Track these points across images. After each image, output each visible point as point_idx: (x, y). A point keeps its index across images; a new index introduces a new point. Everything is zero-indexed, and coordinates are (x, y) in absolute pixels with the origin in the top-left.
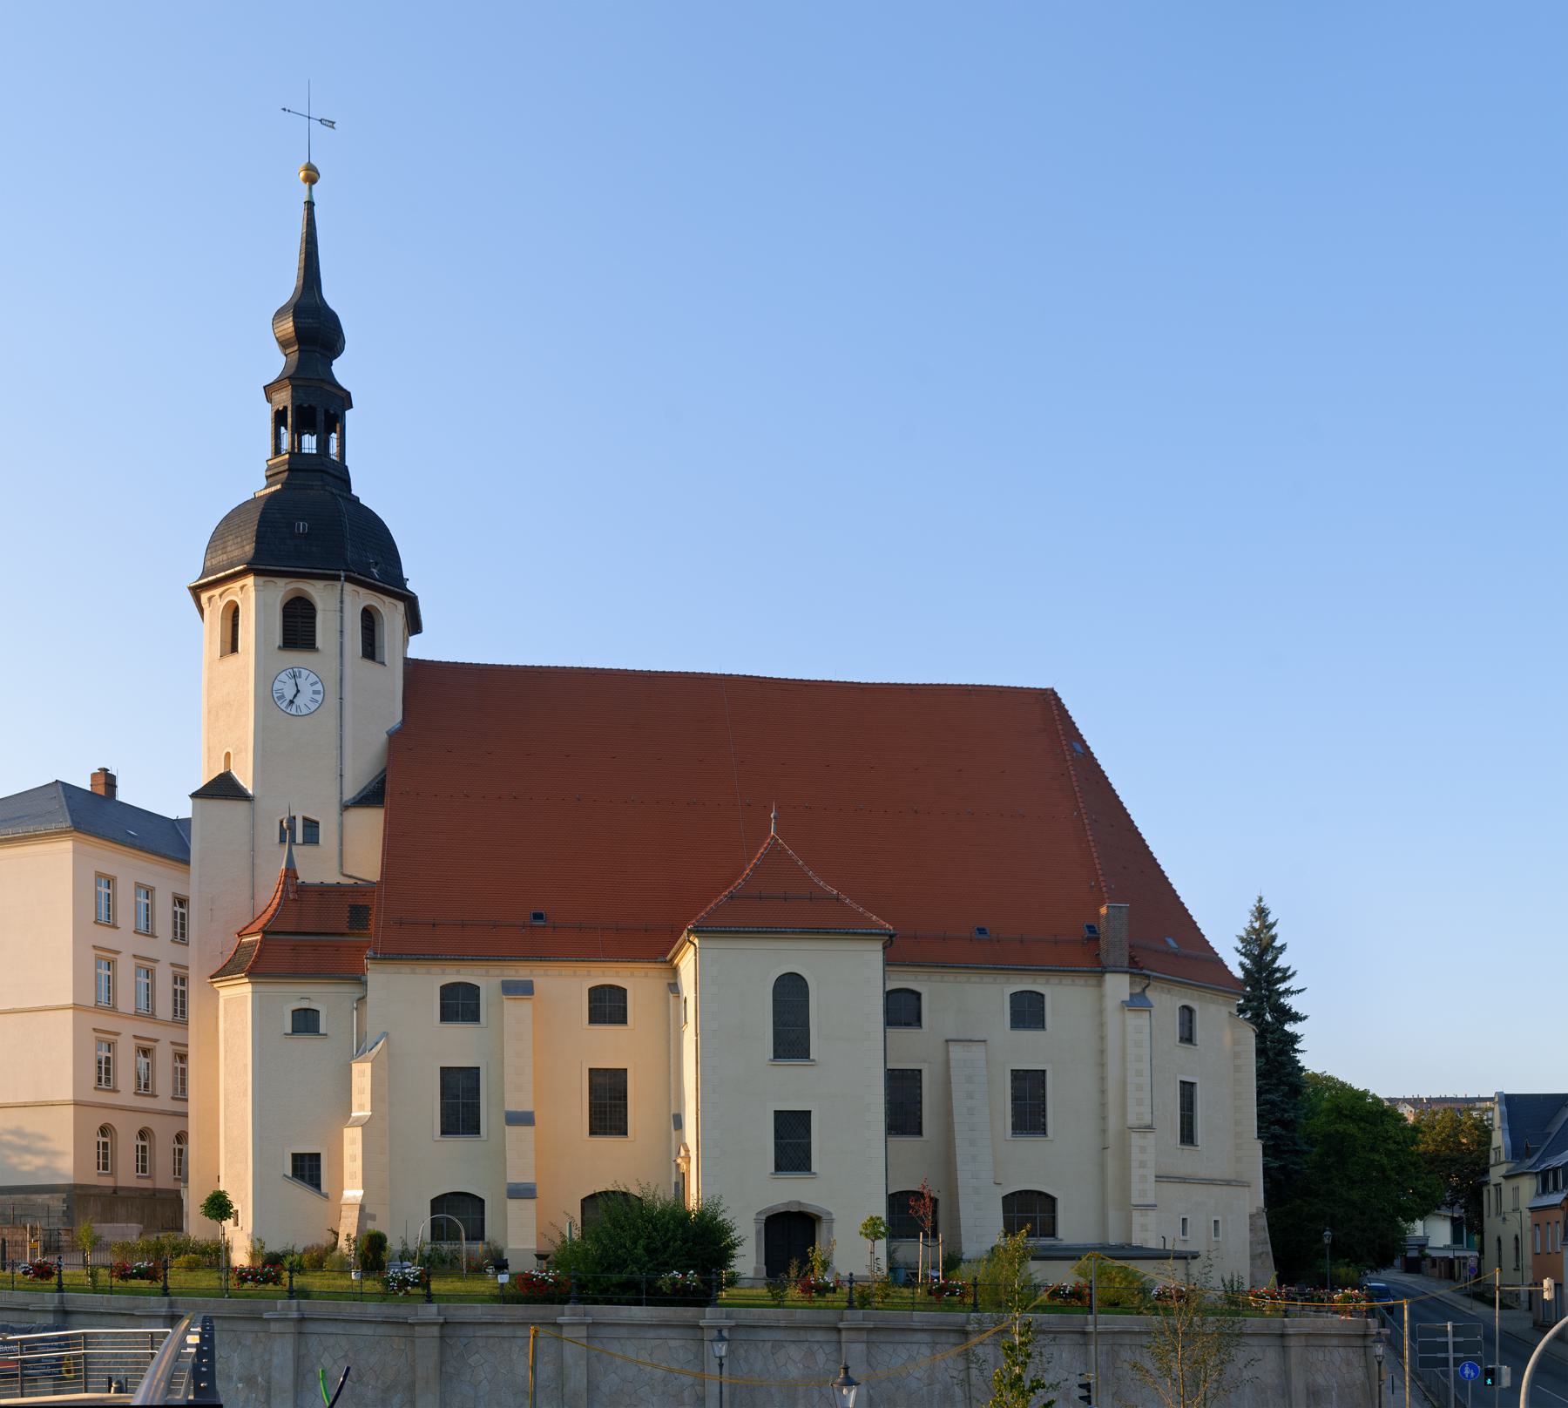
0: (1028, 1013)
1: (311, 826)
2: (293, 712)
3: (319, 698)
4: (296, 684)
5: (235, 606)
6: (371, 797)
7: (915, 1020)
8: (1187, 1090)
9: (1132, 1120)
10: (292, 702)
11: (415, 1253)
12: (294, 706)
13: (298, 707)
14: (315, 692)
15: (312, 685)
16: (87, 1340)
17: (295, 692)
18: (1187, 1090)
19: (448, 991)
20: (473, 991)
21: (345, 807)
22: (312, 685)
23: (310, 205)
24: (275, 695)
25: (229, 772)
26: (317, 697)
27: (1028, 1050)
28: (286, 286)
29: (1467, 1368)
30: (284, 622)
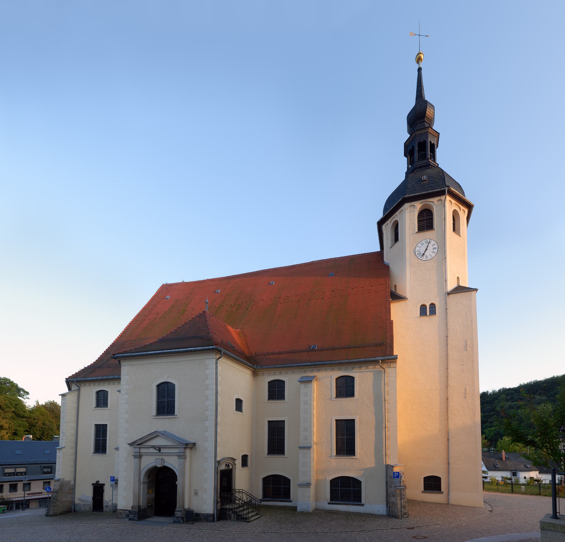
1: (433, 306)
2: (424, 259)
3: (436, 251)
4: (428, 246)
5: (397, 223)
10: (424, 254)
11: (214, 514)
12: (425, 256)
13: (426, 256)
14: (434, 249)
15: (433, 246)
19: (272, 384)
22: (433, 246)
23: (420, 70)
24: (416, 253)
25: (459, 285)
26: (434, 250)
29: (47, 488)
30: (432, 221)
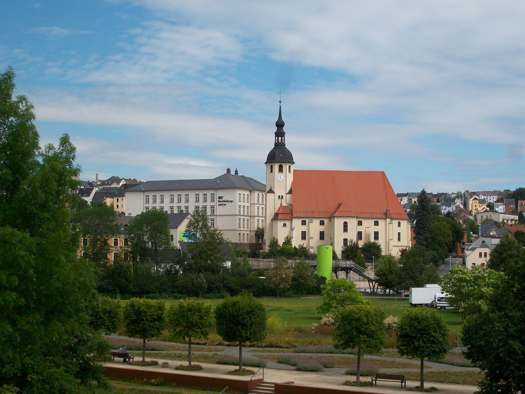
0: (376, 224)
1: (282, 196)
6: (290, 192)
7: (361, 225)
8: (399, 234)
9: (390, 239)
16: (347, 383)
17: (13, 391)
18: (399, 234)
20: (285, 224)
21: (287, 194)
23: (280, 106)
27: (376, 228)
28: (277, 119)
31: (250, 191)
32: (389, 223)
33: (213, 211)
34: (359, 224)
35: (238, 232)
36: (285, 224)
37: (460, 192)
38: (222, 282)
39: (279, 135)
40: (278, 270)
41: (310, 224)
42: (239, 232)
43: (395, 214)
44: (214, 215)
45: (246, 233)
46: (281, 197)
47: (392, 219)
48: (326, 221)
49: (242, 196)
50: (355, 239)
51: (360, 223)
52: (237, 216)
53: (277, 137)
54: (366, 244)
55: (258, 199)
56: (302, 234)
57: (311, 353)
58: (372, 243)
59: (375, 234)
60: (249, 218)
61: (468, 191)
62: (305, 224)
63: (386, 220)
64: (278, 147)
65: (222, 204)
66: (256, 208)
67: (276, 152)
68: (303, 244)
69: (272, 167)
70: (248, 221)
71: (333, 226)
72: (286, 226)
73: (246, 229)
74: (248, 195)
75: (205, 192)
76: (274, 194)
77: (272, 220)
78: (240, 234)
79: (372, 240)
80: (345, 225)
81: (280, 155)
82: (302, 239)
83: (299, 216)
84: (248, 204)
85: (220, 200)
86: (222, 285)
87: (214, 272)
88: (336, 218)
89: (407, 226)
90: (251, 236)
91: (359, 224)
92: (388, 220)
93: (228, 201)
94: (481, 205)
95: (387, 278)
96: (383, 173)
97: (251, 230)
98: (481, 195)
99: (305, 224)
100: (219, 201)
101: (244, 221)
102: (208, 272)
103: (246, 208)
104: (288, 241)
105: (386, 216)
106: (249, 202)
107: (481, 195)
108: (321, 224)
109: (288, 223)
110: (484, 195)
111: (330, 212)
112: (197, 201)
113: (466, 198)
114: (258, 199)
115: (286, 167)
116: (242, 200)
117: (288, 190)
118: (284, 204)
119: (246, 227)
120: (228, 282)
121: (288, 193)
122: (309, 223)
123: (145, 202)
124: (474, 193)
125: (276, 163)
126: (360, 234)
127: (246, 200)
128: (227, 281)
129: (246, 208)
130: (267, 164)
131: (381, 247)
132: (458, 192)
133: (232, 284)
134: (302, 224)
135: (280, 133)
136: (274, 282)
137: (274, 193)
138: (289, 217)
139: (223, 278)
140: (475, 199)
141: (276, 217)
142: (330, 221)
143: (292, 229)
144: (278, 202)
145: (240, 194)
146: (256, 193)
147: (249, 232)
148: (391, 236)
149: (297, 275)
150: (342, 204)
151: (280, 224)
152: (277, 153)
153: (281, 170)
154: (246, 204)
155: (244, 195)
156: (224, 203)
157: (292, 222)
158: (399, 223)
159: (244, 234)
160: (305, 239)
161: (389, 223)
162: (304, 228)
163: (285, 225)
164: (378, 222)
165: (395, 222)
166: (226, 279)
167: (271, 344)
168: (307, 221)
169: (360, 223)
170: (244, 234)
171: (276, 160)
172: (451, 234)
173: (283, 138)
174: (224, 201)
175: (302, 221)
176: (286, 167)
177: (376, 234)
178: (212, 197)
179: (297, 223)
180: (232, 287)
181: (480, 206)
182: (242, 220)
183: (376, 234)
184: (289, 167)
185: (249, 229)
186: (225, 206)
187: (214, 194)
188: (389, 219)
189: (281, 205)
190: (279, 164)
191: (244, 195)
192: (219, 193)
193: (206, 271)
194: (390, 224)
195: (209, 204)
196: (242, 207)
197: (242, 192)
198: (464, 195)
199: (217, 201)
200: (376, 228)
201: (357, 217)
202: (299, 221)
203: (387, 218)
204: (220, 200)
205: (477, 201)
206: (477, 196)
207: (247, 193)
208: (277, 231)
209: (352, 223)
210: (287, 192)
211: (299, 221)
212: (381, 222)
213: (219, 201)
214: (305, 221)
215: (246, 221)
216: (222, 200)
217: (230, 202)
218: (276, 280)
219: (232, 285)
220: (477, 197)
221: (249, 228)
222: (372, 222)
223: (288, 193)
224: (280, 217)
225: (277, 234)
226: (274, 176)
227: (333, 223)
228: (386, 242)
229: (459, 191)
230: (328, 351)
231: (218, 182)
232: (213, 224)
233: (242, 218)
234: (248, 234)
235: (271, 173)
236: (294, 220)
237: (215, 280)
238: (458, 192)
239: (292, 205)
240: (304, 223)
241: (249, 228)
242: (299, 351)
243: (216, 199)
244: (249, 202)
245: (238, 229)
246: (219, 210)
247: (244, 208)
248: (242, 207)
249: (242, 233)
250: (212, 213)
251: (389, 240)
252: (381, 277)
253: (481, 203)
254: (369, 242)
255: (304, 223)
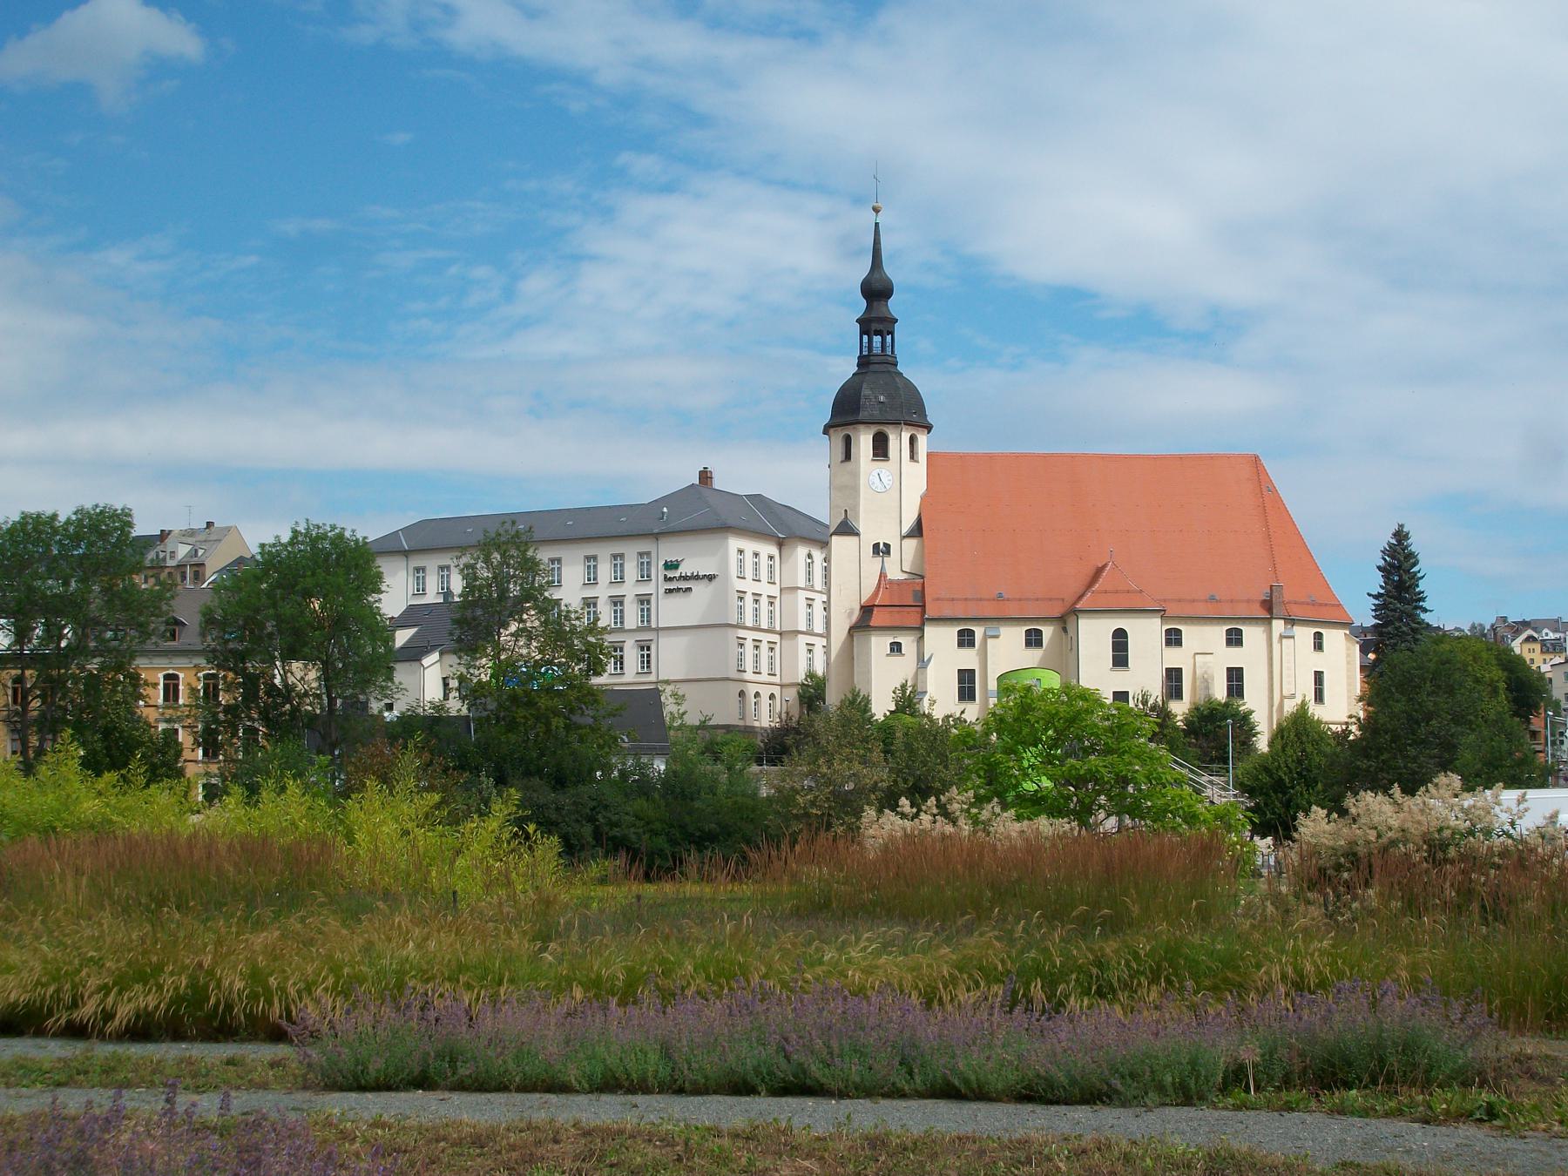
1: (887, 546)
6: (917, 531)
7: (1179, 643)
8: (1319, 677)
18: (1319, 677)
20: (899, 644)
27: (1234, 657)
28: (863, 269)
31: (780, 544)
32: (1282, 637)
33: (646, 614)
34: (1169, 643)
35: (735, 688)
36: (899, 644)
37: (1481, 625)
38: (592, 820)
39: (874, 326)
40: (821, 761)
41: (990, 642)
42: (739, 687)
43: (1302, 603)
44: (649, 629)
45: (765, 692)
46: (882, 550)
47: (1291, 621)
48: (1048, 632)
49: (749, 559)
50: (1156, 691)
51: (1174, 639)
52: (730, 630)
53: (865, 338)
54: (1196, 709)
55: (809, 573)
56: (961, 681)
57: (527, 1087)
58: (1220, 704)
59: (1229, 679)
60: (776, 638)
61: (1504, 619)
62: (971, 644)
63: (1270, 623)
64: (873, 368)
65: (679, 590)
66: (802, 604)
67: (865, 386)
68: (963, 712)
69: (848, 441)
70: (772, 649)
71: (1075, 648)
72: (900, 650)
73: (764, 677)
74: (771, 558)
75: (618, 548)
76: (855, 539)
77: (850, 630)
78: (742, 694)
79: (1220, 693)
80: (1120, 641)
81: (876, 397)
82: (874, 553)
83: (948, 613)
84: (774, 590)
85: (670, 574)
86: (587, 830)
87: (560, 782)
88: (1086, 615)
89: (1348, 649)
90: (784, 702)
91: (1169, 643)
92: (1278, 626)
93: (697, 578)
94: (1547, 657)
95: (1289, 801)
96: (1256, 458)
97: (785, 681)
98: (1546, 630)
99: (971, 644)
100: (667, 579)
101: (757, 647)
102: (536, 781)
103: (764, 601)
104: (907, 702)
105: (1269, 609)
106: (777, 581)
107: (1546, 630)
108: (1028, 644)
109: (907, 642)
110: (1556, 630)
111: (1063, 600)
112: (589, 579)
113: (1499, 638)
114: (809, 573)
115: (898, 441)
116: (749, 573)
117: (908, 522)
118: (894, 574)
119: (764, 668)
120: (615, 818)
121: (910, 535)
122: (986, 637)
123: (410, 593)
124: (1525, 624)
125: (861, 427)
126: (1173, 677)
127: (764, 575)
128: (609, 815)
129: (764, 601)
130: (832, 431)
131: (1255, 717)
132: (1473, 624)
133: (634, 825)
134: (961, 644)
135: (876, 323)
136: (807, 815)
137: (857, 534)
138: (912, 618)
139: (594, 803)
140: (1530, 639)
141: (865, 622)
142: (1065, 630)
143: (922, 663)
144: (872, 566)
145: (741, 552)
146: (801, 551)
147: (776, 691)
148: (1289, 683)
149: (905, 781)
150: (1105, 566)
151: (879, 644)
152: (866, 392)
153: (880, 449)
154: (766, 589)
155: (756, 555)
156: (684, 585)
157: (922, 637)
158: (1318, 637)
159: (757, 695)
160: (972, 697)
161: (1282, 637)
162: (968, 659)
163: (896, 648)
164: (1240, 632)
165: (1305, 634)
166: (606, 807)
167: (198, 995)
168: (979, 632)
169: (1174, 639)
170: (757, 695)
171: (863, 415)
172: (1502, 685)
173: (889, 338)
174: (685, 578)
175: (961, 633)
176: (898, 441)
177: (1235, 677)
178: (642, 563)
179: (940, 639)
180: (633, 838)
181: (1545, 660)
182: (749, 645)
183: (1235, 677)
184: (913, 440)
185: (776, 679)
186: (688, 593)
187: (648, 554)
188: (1283, 622)
189: (882, 575)
190: (874, 429)
191: (756, 555)
192: (668, 550)
193: (528, 774)
194: (1284, 640)
195: (630, 590)
196: (749, 599)
197: (750, 546)
198: (1494, 630)
199: (661, 578)
200: (1234, 657)
201: (1162, 614)
202: (950, 633)
203: (1272, 618)
204: (670, 574)
205: (1537, 647)
206: (1535, 629)
207: (770, 549)
208: (869, 672)
209: (1145, 634)
210: (905, 530)
211: (950, 633)
212: (1252, 635)
213: (667, 579)
214: (971, 633)
215: (764, 647)
216: (677, 575)
217: (706, 580)
218: (813, 803)
219: (632, 830)
220: (1536, 635)
221: (778, 673)
222: (1218, 633)
223: (910, 535)
224: (877, 618)
225: (869, 682)
226: (855, 475)
227: (1074, 638)
228: (1271, 706)
229: (1477, 623)
230: (747, 1057)
231: (665, 510)
232: (648, 662)
233: (750, 636)
234: (772, 697)
235: (847, 463)
236: (929, 631)
237: (557, 809)
238: (1473, 624)
239: (923, 577)
240: (966, 639)
241: (778, 673)
242: (376, 1066)
243: (658, 571)
244: (777, 581)
245: (733, 674)
246: (670, 611)
247: (756, 601)
248: (749, 599)
249: (751, 689)
250: (642, 621)
251: (1283, 698)
252: (1266, 794)
253: (1548, 652)
254: (1210, 700)
255: (966, 639)
